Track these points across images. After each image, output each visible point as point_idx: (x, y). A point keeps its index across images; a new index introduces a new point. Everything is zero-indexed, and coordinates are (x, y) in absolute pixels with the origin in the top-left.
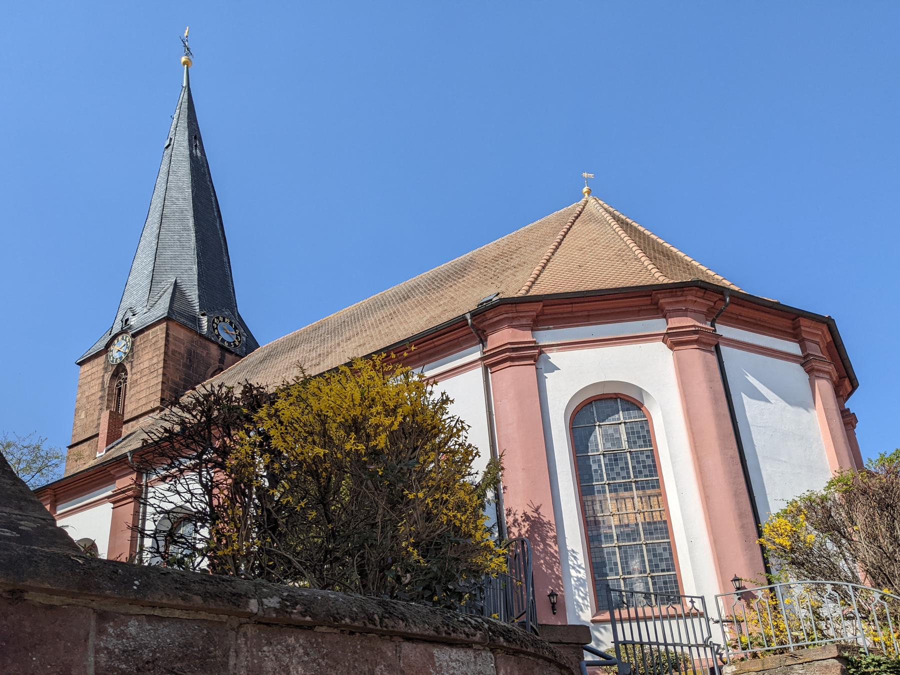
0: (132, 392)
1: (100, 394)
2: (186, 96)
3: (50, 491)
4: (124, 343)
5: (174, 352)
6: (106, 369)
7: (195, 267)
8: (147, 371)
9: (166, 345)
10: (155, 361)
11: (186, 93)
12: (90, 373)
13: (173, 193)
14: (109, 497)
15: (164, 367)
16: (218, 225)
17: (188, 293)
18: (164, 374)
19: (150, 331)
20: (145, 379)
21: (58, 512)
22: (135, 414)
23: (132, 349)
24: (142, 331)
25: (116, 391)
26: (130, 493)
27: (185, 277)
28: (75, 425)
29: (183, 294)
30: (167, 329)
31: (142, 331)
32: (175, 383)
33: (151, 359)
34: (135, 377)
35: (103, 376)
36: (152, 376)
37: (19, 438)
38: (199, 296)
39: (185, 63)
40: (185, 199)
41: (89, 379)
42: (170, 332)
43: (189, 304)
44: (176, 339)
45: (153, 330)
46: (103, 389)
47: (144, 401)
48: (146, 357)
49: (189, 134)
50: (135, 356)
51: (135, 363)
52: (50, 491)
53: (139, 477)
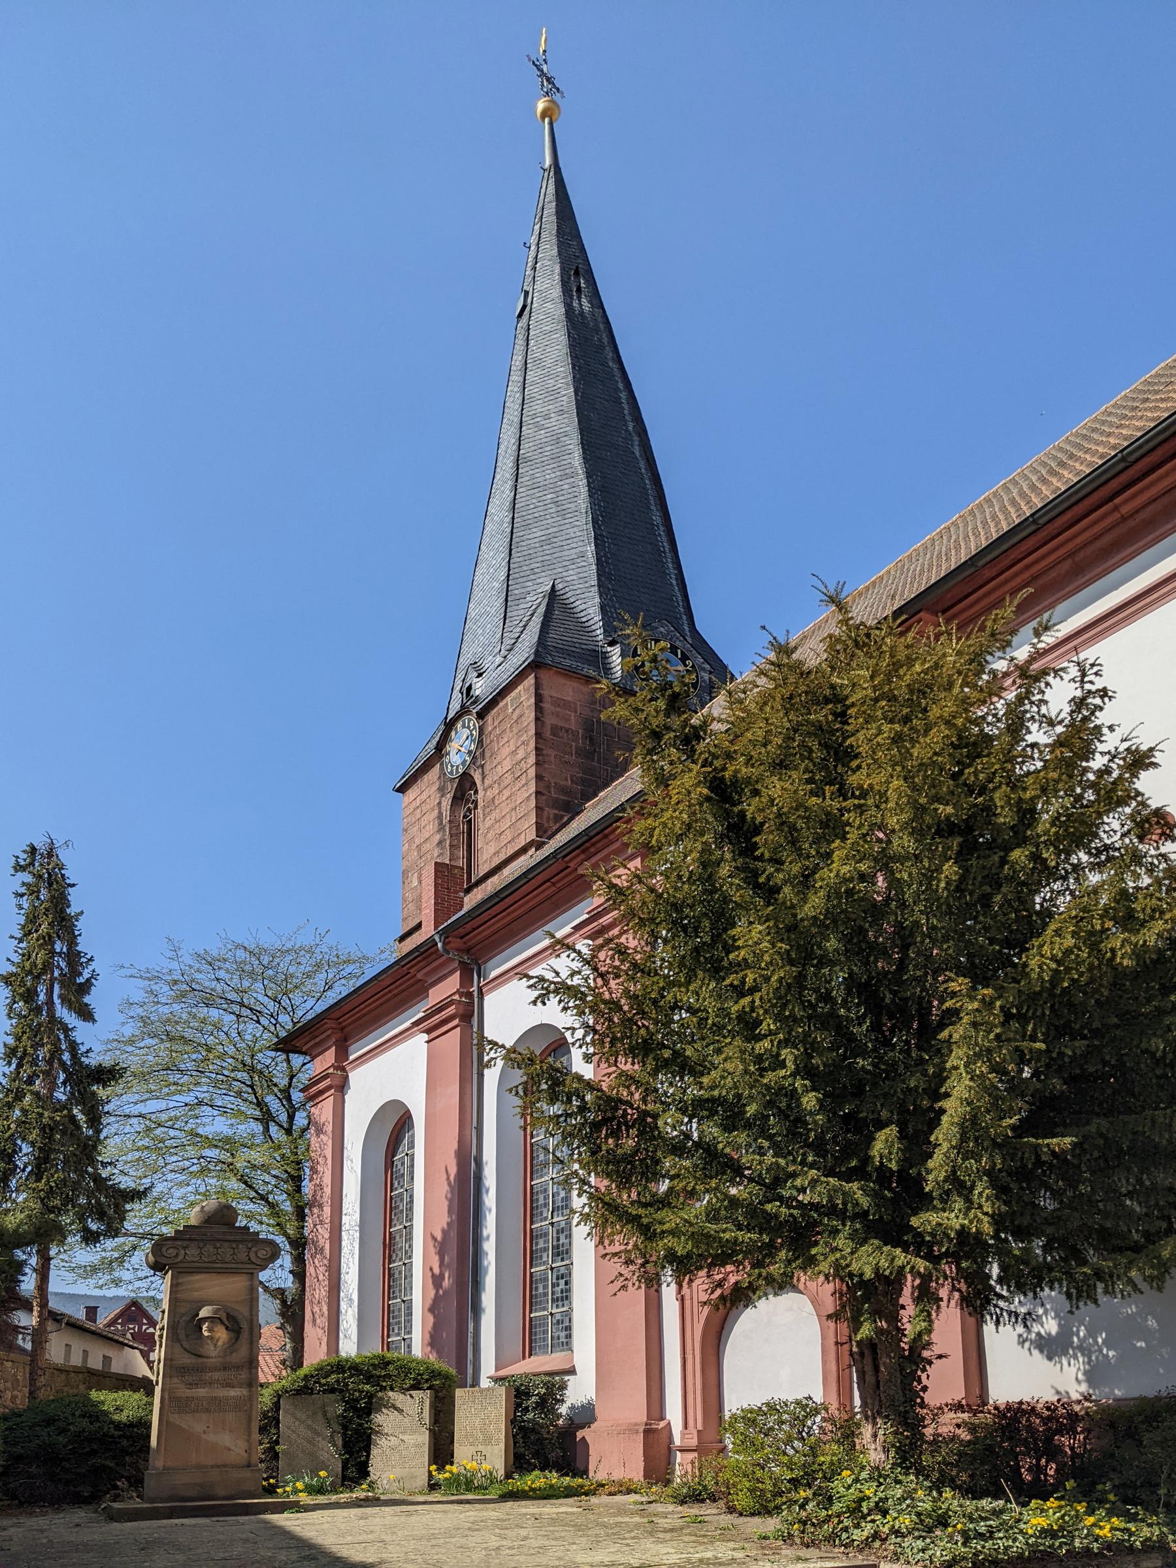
0: (488, 823)
1: (438, 837)
2: (551, 189)
3: (330, 1024)
4: (466, 732)
5: (555, 730)
6: (442, 790)
7: (591, 549)
8: (509, 778)
9: (537, 719)
10: (521, 754)
11: (552, 181)
12: (418, 801)
13: (537, 407)
14: (416, 1024)
15: (537, 764)
16: (637, 450)
17: (579, 605)
18: (539, 777)
19: (508, 699)
20: (506, 793)
21: (352, 1058)
22: (497, 861)
23: (480, 742)
24: (493, 703)
25: (463, 827)
26: (451, 1010)
27: (572, 575)
28: (404, 900)
29: (568, 609)
30: (538, 686)
31: (493, 703)
32: (563, 790)
33: (514, 752)
34: (490, 794)
35: (440, 803)
36: (519, 785)
37: (280, 937)
38: (603, 608)
39: (544, 114)
40: (561, 412)
41: (418, 813)
42: (546, 692)
43: (583, 628)
44: (557, 702)
45: (513, 694)
46: (441, 828)
47: (508, 836)
48: (506, 751)
49: (563, 269)
50: (487, 755)
51: (487, 767)
52: (330, 1024)
53: (466, 979)
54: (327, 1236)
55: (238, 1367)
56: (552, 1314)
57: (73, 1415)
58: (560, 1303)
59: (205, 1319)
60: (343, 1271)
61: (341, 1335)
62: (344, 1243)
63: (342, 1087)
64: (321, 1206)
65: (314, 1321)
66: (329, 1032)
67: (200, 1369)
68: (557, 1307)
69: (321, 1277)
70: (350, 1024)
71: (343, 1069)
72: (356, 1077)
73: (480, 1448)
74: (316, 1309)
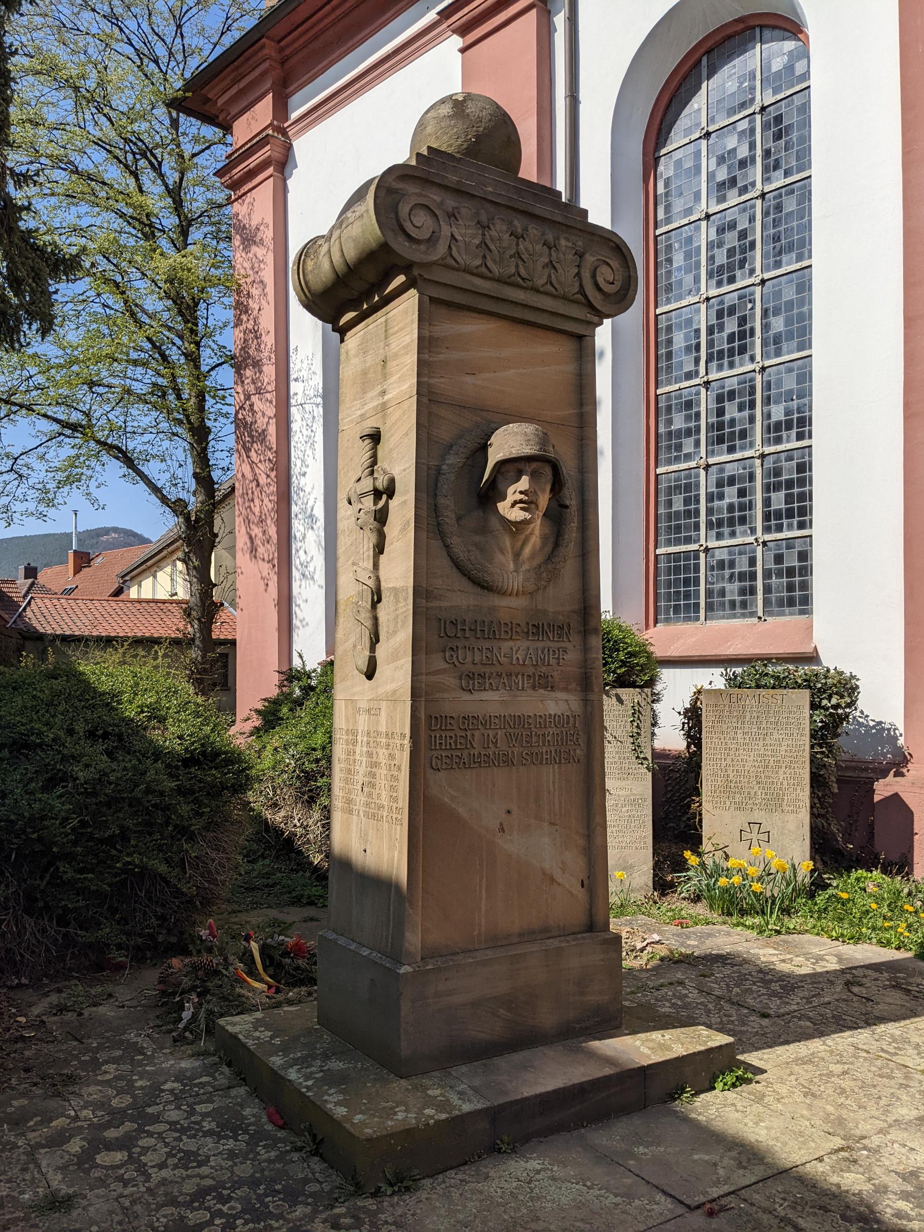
21: (294, 116)
54: (271, 412)
55: (561, 630)
56: (707, 550)
57: (71, 732)
58: (726, 530)
59: (512, 467)
60: (296, 470)
61: (296, 574)
62: (295, 427)
63: (283, 163)
64: (257, 364)
65: (253, 550)
66: (266, 65)
67: (488, 630)
68: (719, 536)
69: (263, 480)
70: (297, 52)
71: (284, 132)
72: (305, 146)
73: (757, 816)
74: (256, 531)
